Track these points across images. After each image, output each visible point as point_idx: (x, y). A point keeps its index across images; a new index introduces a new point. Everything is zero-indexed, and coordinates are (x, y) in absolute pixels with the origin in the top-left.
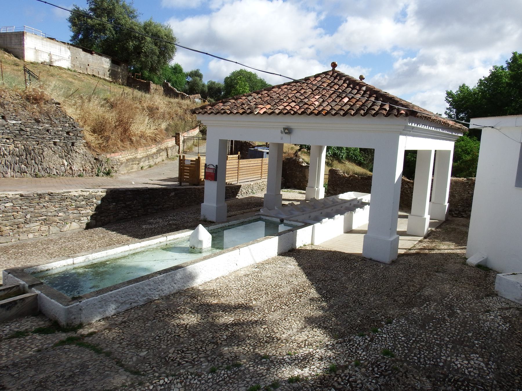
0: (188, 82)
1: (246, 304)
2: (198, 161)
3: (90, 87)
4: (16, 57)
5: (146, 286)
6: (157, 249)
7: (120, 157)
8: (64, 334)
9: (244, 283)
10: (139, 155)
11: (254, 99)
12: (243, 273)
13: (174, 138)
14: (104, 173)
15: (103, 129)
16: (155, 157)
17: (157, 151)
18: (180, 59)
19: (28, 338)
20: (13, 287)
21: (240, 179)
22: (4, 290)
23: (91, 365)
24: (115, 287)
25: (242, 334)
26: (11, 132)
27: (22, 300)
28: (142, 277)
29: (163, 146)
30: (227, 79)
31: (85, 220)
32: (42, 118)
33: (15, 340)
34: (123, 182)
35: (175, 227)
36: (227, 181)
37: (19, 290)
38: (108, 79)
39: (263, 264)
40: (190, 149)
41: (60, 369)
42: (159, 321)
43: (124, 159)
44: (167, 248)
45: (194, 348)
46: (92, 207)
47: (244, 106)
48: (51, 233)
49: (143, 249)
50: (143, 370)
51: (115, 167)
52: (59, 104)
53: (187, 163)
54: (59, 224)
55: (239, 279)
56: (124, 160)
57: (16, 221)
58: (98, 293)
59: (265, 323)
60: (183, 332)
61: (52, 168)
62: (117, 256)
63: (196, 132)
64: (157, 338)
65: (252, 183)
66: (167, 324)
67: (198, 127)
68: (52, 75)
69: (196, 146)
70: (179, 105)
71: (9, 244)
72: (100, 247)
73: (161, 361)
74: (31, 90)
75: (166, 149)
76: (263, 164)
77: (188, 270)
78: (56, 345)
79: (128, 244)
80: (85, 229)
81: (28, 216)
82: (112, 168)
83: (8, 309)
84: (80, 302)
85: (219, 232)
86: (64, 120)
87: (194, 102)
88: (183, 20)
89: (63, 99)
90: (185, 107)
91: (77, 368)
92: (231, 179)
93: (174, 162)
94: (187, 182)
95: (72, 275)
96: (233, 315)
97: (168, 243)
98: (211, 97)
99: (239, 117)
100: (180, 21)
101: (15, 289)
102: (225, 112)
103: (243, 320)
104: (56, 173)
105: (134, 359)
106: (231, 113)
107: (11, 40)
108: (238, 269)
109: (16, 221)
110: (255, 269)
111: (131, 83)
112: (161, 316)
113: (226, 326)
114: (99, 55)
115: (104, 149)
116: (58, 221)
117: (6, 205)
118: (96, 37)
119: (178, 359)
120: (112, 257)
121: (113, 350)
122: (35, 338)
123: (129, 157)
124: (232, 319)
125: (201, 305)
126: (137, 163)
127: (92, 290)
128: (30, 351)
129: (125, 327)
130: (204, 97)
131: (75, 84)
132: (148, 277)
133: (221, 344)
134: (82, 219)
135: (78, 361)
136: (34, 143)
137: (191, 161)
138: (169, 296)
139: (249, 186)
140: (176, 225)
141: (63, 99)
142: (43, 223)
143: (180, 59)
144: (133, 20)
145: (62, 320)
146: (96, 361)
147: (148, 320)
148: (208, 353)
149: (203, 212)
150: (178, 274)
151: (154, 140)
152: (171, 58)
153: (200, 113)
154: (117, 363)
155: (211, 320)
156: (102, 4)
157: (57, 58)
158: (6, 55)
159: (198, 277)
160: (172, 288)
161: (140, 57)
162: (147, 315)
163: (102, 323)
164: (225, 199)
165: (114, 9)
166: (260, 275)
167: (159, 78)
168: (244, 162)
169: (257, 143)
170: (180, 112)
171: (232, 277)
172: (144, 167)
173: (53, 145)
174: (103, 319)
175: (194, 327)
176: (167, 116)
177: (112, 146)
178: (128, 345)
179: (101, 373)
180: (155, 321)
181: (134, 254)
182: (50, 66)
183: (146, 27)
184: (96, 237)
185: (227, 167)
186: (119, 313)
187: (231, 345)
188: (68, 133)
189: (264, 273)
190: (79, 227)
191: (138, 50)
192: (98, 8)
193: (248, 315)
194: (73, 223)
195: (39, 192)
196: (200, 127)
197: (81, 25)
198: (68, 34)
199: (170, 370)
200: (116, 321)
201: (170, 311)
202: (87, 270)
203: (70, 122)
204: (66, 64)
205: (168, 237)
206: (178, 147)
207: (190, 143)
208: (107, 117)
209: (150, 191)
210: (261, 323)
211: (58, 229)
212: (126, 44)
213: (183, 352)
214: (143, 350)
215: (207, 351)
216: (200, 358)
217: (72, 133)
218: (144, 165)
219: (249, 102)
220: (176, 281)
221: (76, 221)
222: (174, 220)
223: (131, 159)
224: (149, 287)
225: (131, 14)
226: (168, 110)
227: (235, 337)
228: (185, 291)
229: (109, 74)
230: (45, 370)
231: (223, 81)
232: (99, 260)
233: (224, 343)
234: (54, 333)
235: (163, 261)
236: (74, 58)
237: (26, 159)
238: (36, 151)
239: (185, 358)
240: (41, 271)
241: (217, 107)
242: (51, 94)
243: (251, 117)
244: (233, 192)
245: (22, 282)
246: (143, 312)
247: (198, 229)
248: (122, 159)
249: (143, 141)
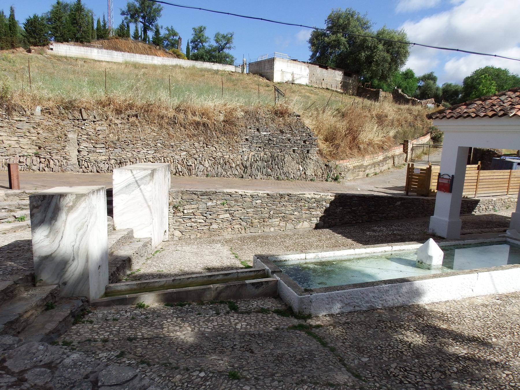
0: (419, 87)
1: (484, 339)
2: (429, 170)
3: (324, 100)
4: (268, 79)
5: (370, 292)
6: (381, 257)
7: (348, 163)
8: (296, 320)
9: (481, 313)
10: (365, 162)
11: (510, 99)
12: (479, 301)
14: (332, 179)
15: (334, 138)
16: (381, 165)
17: (384, 159)
18: (415, 64)
19: (269, 315)
20: (261, 270)
21: (478, 192)
22: (254, 271)
23: (318, 355)
24: (342, 288)
25: (477, 372)
26: (262, 142)
27: (267, 282)
28: (367, 283)
29: (390, 154)
30: (467, 78)
31: (315, 221)
32: (286, 129)
33: (260, 315)
34: (349, 188)
35: (399, 237)
36: (464, 194)
37: (265, 273)
38: (339, 91)
39: (507, 296)
40: (419, 157)
41: (292, 350)
42: (381, 332)
44: (391, 258)
45: (418, 371)
47: (494, 108)
49: (367, 255)
50: (364, 375)
51: (343, 173)
52: (299, 116)
53: (416, 172)
55: (475, 308)
56: (351, 167)
57: (263, 215)
58: (327, 289)
59: (508, 369)
60: (406, 350)
61: (290, 172)
62: (343, 258)
63: (427, 139)
64: (379, 348)
65: (494, 199)
66: (389, 337)
67: (430, 134)
68: (294, 92)
69: (426, 154)
70: (410, 111)
71: (257, 234)
72: (327, 247)
73: (382, 373)
74: (279, 106)
75: (393, 157)
76: (512, 176)
77: (415, 285)
78: (290, 328)
79: (354, 248)
80: (314, 229)
81: (272, 213)
83: (256, 288)
84: (311, 294)
85: (451, 249)
86: (303, 130)
87: (426, 107)
88: (418, 22)
89: (303, 111)
90: (416, 113)
91: (306, 354)
92: (468, 193)
93: (400, 170)
94: (415, 192)
95: (304, 268)
96: (466, 347)
97: (393, 253)
98: (447, 101)
99: (486, 121)
100: (414, 24)
101: (261, 272)
102: (469, 116)
103: (479, 357)
105: (356, 362)
106: (477, 116)
107: (265, 66)
108: (474, 296)
109: (263, 215)
110: (497, 301)
111: (361, 92)
112: (383, 327)
113: (457, 358)
114: (334, 69)
115: (334, 156)
117: (257, 202)
118: (331, 54)
119: (401, 377)
120: (338, 258)
121: (336, 347)
122: (274, 317)
123: (356, 164)
124: (465, 352)
125: (427, 326)
126: (363, 170)
127: (320, 286)
128: (271, 327)
129: (348, 328)
130: (438, 101)
131: (312, 98)
132: (373, 284)
133: (450, 375)
134: (313, 219)
135: (307, 348)
136: (278, 150)
137: (421, 170)
138: (392, 308)
139: (490, 202)
140: (401, 235)
141: (303, 111)
143: (415, 64)
144: (367, 31)
145: (296, 307)
146: (322, 352)
147: (370, 327)
148: (435, 381)
149: (431, 226)
150: (404, 287)
151: (382, 148)
152: (403, 63)
153: (437, 117)
154: (340, 361)
155: (438, 345)
156: (338, 21)
157: (298, 77)
158: (261, 79)
159: (425, 295)
160: (396, 300)
161: (371, 66)
162: (369, 322)
163: (328, 318)
164: (461, 213)
165: (349, 23)
166: (503, 308)
167: (389, 86)
168: (486, 174)
169: (504, 151)
170: (410, 118)
171: (466, 304)
172: (374, 174)
173: (292, 152)
174: (329, 315)
175: (419, 348)
176: (396, 123)
177: (341, 154)
178: (351, 346)
179: (326, 366)
180: (377, 330)
181: (359, 259)
182: (292, 84)
183: (379, 37)
184: (324, 238)
185: (466, 178)
186: (343, 313)
187: (462, 381)
188: (305, 142)
189: (509, 308)
190: (309, 226)
191: (369, 60)
192: (335, 26)
193: (486, 352)
195: (281, 193)
196: (431, 133)
197: (319, 44)
198: (308, 54)
199: (391, 385)
200: (340, 320)
201: (393, 324)
202: (316, 266)
203: (307, 132)
204: (304, 81)
206: (405, 155)
207: (419, 151)
208: (338, 126)
209: (356, 199)
210: (503, 367)
212: (358, 56)
213: (406, 370)
214: (365, 356)
215: (433, 378)
216: (425, 383)
217: (308, 141)
218: (369, 172)
219: (501, 103)
220: (401, 295)
221: (308, 220)
222: (399, 230)
224: (374, 295)
225: (364, 25)
226: (397, 117)
227: (468, 373)
228: (409, 307)
229: (341, 86)
230: (282, 347)
231: (462, 81)
232: (326, 259)
233: (453, 376)
234: (288, 317)
235: (387, 271)
236: (312, 75)
237: (272, 164)
238: (279, 158)
239: (407, 378)
240: (280, 261)
241: (458, 110)
242: (293, 108)
243: (504, 119)
244: (468, 207)
245: (267, 268)
246: (366, 317)
247: (428, 243)
248: (349, 166)
249: (371, 149)
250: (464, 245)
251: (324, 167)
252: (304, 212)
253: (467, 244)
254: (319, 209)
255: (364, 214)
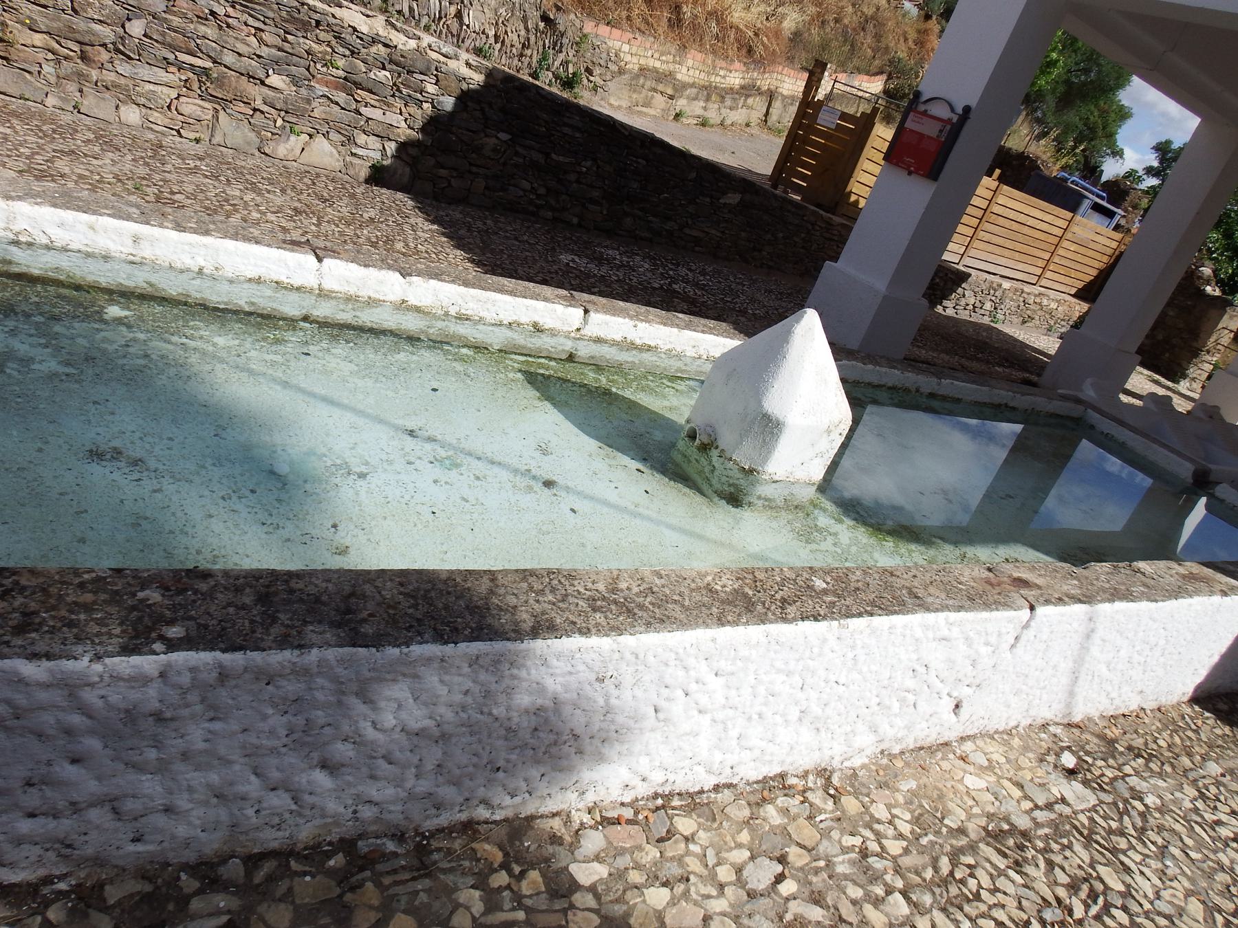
7: (626, 48)
13: (806, 75)
14: (557, 77)
16: (728, 102)
17: (743, 87)
21: (972, 252)
29: (765, 82)
31: (372, 151)
43: (635, 60)
46: (413, 109)
48: (218, 139)
49: (411, 323)
51: (597, 71)
54: (258, 119)
56: (633, 64)
65: (1006, 285)
67: (884, 77)
75: (771, 96)
76: (1069, 235)
81: (136, 28)
82: (588, 70)
97: (584, 351)
104: (406, 10)
109: (79, 24)
116: (259, 103)
126: (670, 91)
134: (362, 139)
142: (196, 86)
159: (610, 752)
190: (338, 165)
194: (321, 143)
196: (890, 77)
205: (595, 317)
211: (252, 135)
218: (688, 110)
221: (334, 136)
222: (696, 285)
223: (656, 70)
247: (786, 338)
248: (628, 58)
250: (932, 395)
251: (534, 16)
252: (321, 89)
253: (944, 398)
254: (399, 104)
255: (596, 194)
